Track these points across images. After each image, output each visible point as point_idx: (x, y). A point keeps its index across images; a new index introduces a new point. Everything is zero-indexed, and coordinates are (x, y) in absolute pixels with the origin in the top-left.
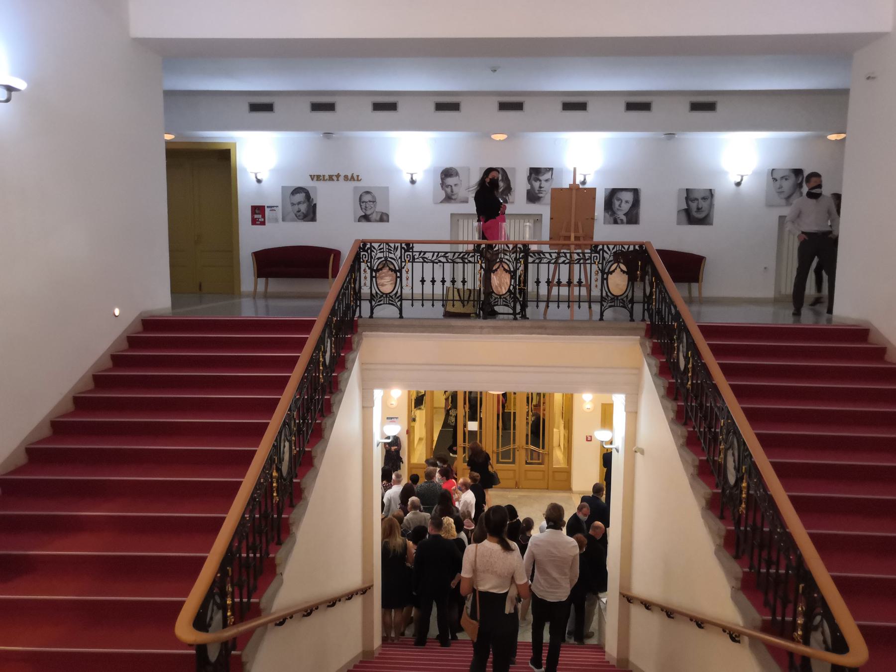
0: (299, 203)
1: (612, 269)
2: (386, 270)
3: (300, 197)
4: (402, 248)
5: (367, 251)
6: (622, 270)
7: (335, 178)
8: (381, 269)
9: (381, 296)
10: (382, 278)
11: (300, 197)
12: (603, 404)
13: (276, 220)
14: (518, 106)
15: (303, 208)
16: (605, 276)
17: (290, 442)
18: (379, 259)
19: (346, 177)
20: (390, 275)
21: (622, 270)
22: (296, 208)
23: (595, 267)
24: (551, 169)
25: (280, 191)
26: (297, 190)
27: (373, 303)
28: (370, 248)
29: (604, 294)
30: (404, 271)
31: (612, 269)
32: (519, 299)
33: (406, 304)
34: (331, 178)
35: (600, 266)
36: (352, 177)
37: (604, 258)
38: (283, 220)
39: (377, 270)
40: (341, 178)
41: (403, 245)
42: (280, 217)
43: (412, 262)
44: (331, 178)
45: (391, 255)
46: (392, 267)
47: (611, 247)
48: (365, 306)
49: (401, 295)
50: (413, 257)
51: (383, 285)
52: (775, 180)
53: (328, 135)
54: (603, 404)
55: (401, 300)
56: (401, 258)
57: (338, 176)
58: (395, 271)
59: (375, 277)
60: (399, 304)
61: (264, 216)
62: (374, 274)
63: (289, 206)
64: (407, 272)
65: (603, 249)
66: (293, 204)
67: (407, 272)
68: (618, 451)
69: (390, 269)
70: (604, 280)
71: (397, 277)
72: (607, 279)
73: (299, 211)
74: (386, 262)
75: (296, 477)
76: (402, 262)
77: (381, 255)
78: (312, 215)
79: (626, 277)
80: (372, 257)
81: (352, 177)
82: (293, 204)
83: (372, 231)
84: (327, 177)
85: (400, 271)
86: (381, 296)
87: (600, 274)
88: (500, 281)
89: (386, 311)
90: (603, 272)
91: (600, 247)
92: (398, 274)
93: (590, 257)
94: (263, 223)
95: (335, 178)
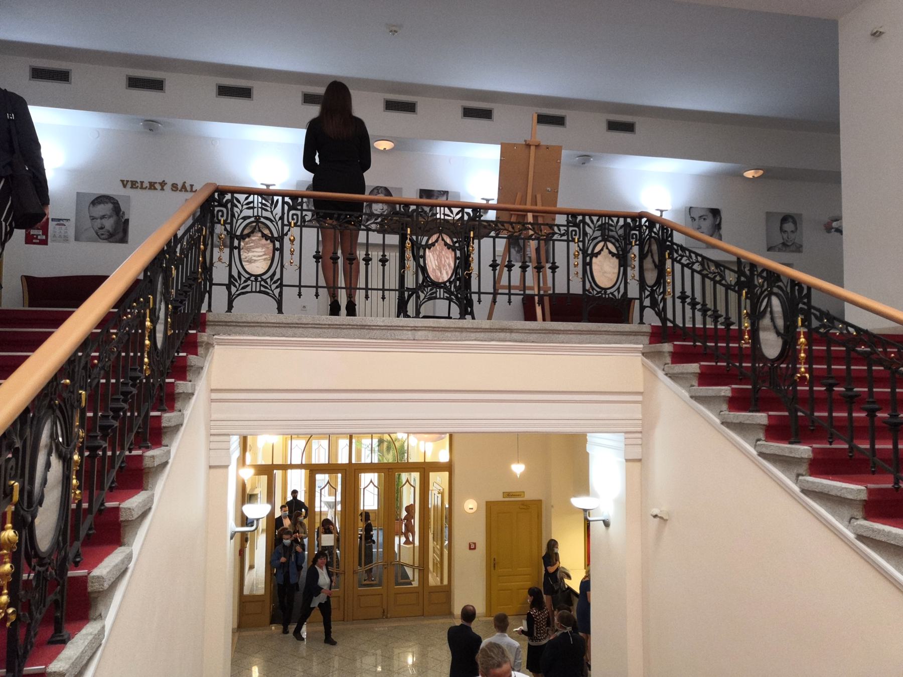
0: (103, 217)
1: (596, 250)
2: (257, 237)
3: (105, 209)
4: (284, 203)
5: (225, 206)
6: (610, 252)
7: (158, 186)
8: (248, 235)
9: (247, 279)
10: (248, 250)
11: (105, 209)
12: (487, 502)
13: (66, 239)
14: (409, 107)
15: (109, 224)
16: (588, 259)
17: (66, 460)
18: (245, 218)
19: (174, 187)
20: (263, 246)
21: (610, 252)
22: (98, 223)
23: (574, 247)
24: (447, 192)
25: (75, 196)
26: (100, 200)
27: (233, 289)
28: (231, 201)
29: (588, 286)
30: (286, 239)
31: (596, 250)
32: (461, 293)
33: (289, 294)
34: (152, 186)
35: (581, 244)
36: (184, 186)
37: (585, 234)
38: (77, 239)
39: (242, 237)
40: (168, 187)
41: (287, 199)
42: (71, 233)
43: (301, 227)
44: (152, 186)
45: (265, 214)
46: (266, 232)
47: (595, 219)
48: (219, 295)
49: (281, 279)
50: (303, 218)
51: (250, 261)
52: (693, 219)
53: (151, 125)
54: (487, 502)
55: (281, 286)
56: (282, 218)
57: (163, 184)
58: (272, 239)
59: (239, 248)
60: (277, 292)
61: (45, 233)
62: (236, 243)
63: (88, 223)
64: (292, 241)
65: (583, 221)
66: (93, 218)
67: (292, 241)
68: (607, 524)
69: (264, 236)
70: (587, 265)
71: (275, 249)
72: (590, 264)
73: (102, 228)
74: (257, 225)
75: (77, 565)
76: (283, 225)
77: (249, 213)
78: (121, 235)
79: (615, 261)
80: (233, 215)
81: (184, 186)
82: (93, 218)
83: (71, 661)
84: (146, 184)
85: (281, 239)
86: (247, 279)
87: (581, 256)
88: (440, 262)
89: (252, 305)
90: (584, 251)
91: (580, 218)
92: (277, 244)
93: (567, 231)
94: (44, 242)
95: (158, 186)
